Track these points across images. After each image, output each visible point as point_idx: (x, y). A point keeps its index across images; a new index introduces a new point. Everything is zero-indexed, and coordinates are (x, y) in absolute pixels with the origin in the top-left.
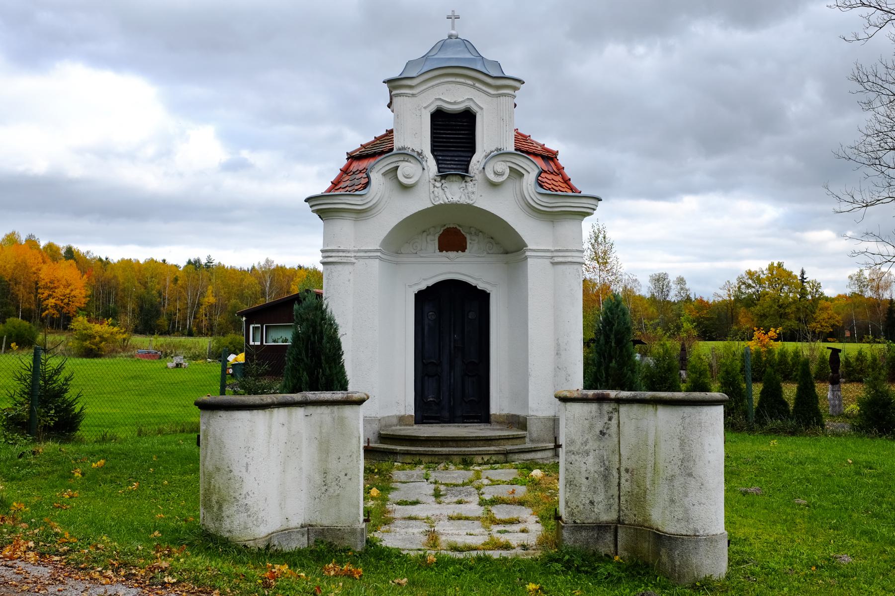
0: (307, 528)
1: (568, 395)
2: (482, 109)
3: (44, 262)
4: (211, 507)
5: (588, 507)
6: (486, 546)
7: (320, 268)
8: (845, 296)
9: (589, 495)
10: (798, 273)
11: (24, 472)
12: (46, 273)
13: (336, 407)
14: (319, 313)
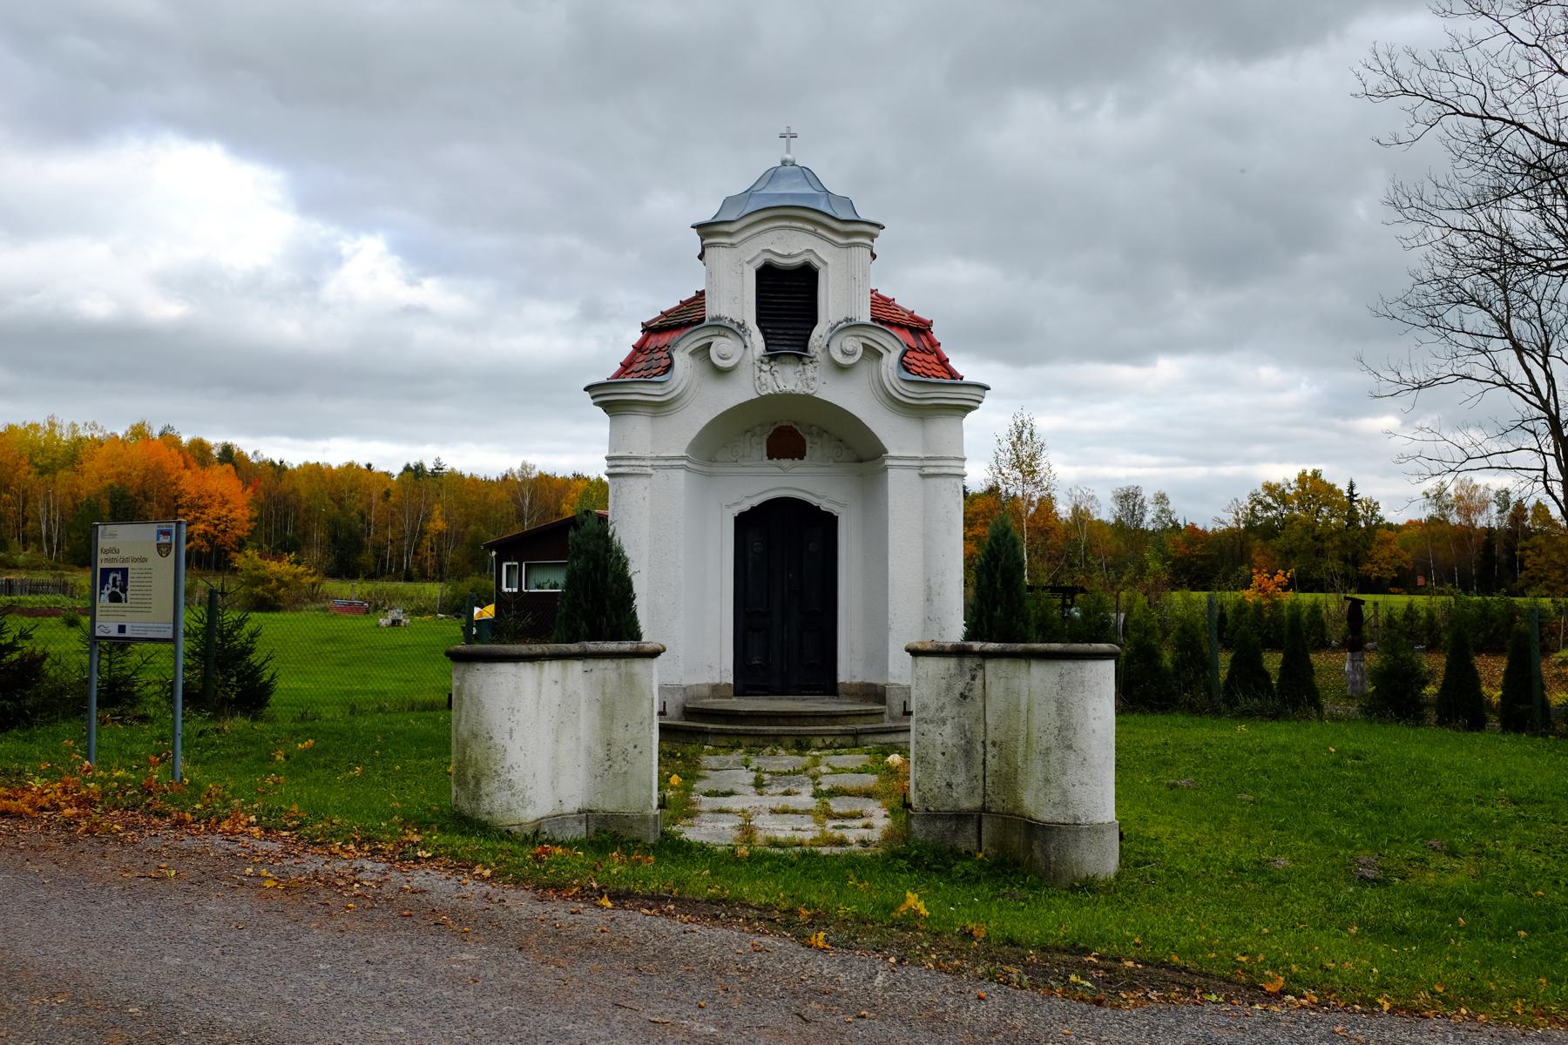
0: (586, 814)
1: (920, 646)
2: (826, 263)
3: (187, 467)
4: (466, 783)
5: (945, 790)
6: (814, 842)
7: (606, 479)
8: (1419, 523)
9: (946, 775)
10: (1343, 487)
11: (208, 754)
12: (190, 483)
14: (602, 542)
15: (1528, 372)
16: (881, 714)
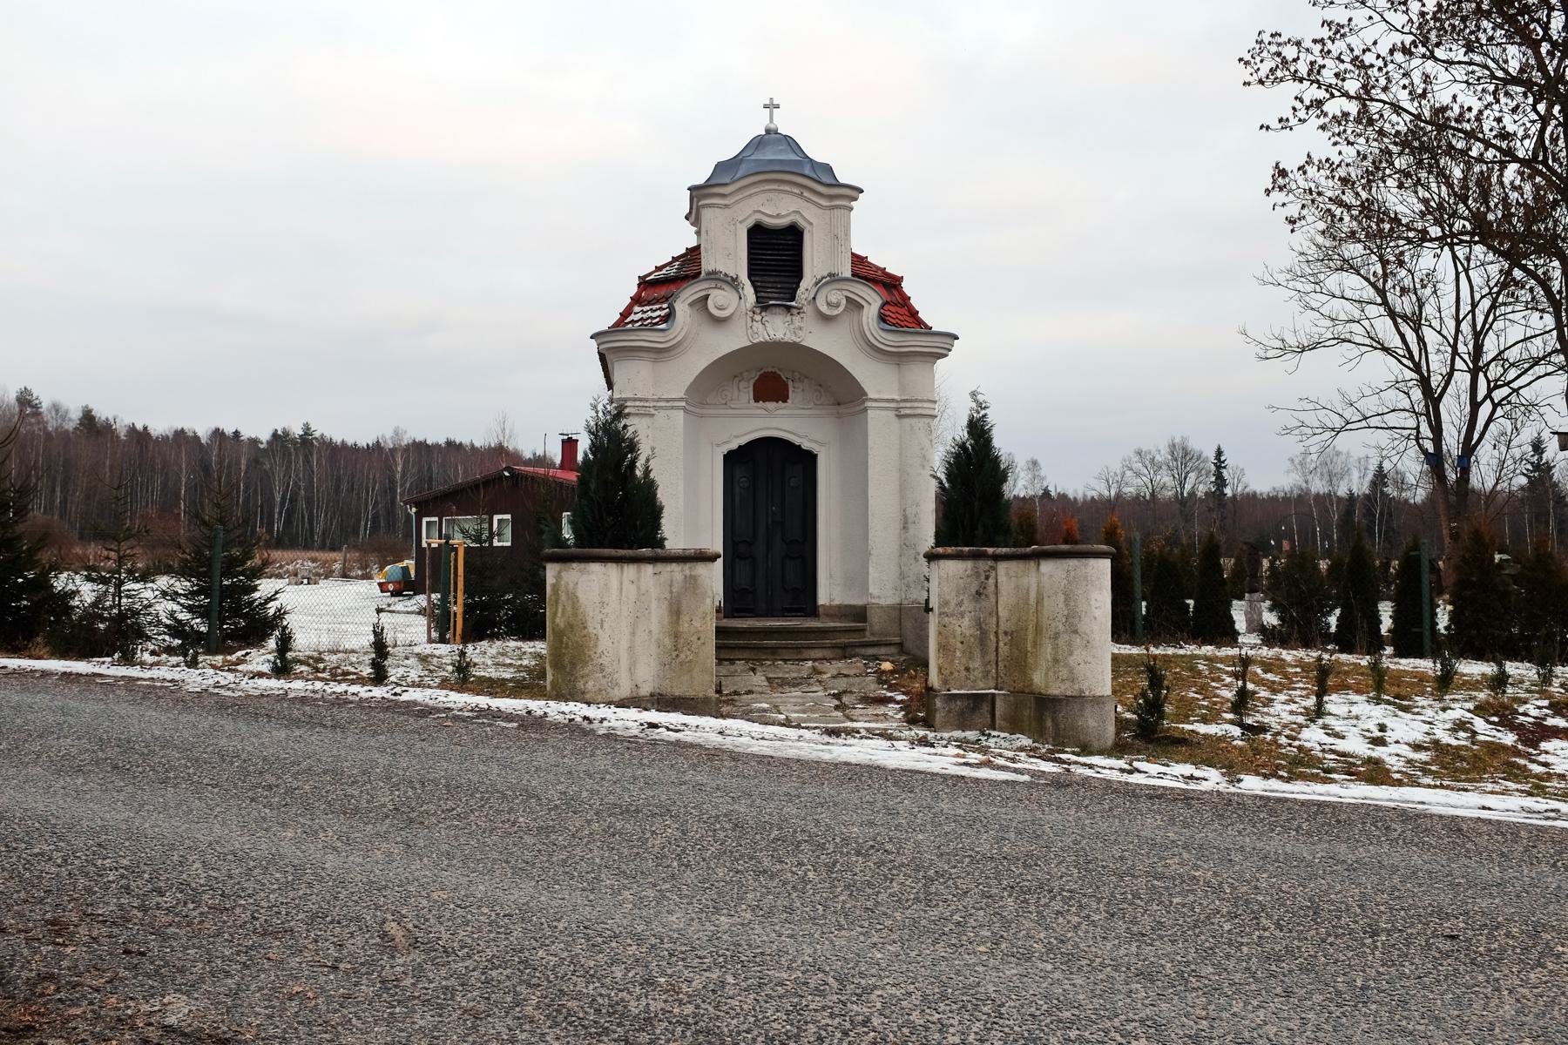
4: (564, 667)
5: (964, 673)
13: (688, 565)
15: (1402, 336)
16: (863, 630)
